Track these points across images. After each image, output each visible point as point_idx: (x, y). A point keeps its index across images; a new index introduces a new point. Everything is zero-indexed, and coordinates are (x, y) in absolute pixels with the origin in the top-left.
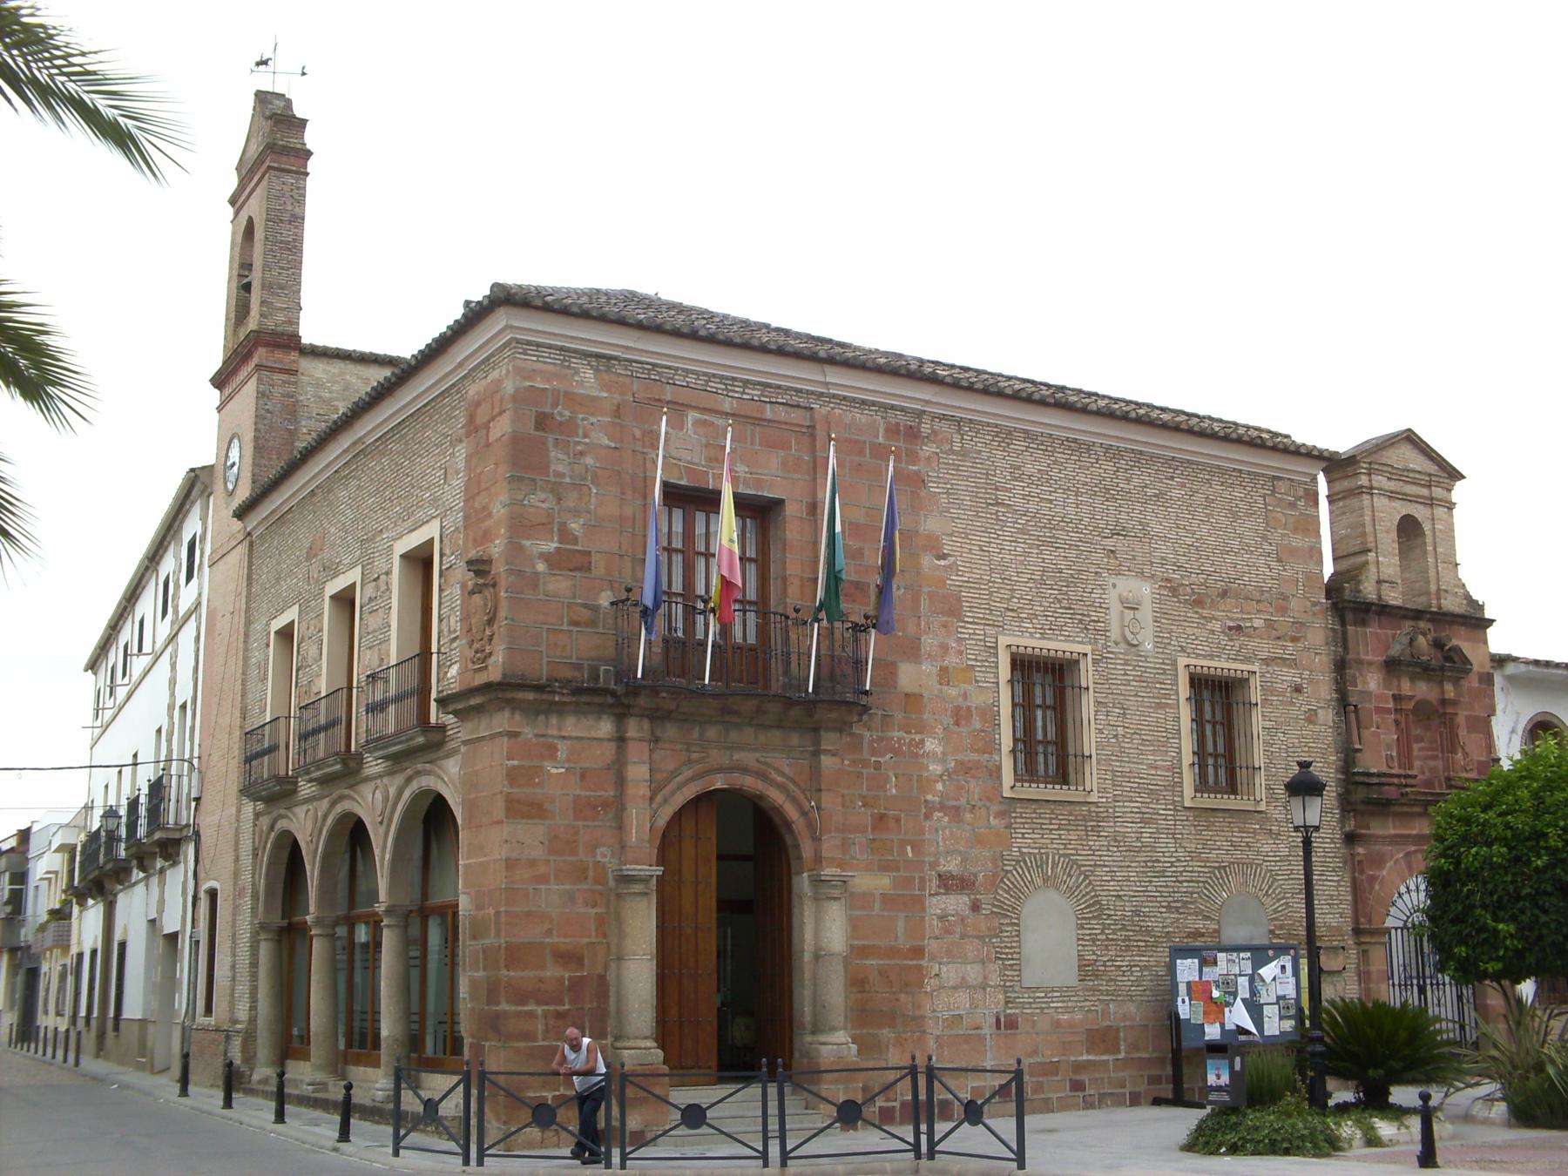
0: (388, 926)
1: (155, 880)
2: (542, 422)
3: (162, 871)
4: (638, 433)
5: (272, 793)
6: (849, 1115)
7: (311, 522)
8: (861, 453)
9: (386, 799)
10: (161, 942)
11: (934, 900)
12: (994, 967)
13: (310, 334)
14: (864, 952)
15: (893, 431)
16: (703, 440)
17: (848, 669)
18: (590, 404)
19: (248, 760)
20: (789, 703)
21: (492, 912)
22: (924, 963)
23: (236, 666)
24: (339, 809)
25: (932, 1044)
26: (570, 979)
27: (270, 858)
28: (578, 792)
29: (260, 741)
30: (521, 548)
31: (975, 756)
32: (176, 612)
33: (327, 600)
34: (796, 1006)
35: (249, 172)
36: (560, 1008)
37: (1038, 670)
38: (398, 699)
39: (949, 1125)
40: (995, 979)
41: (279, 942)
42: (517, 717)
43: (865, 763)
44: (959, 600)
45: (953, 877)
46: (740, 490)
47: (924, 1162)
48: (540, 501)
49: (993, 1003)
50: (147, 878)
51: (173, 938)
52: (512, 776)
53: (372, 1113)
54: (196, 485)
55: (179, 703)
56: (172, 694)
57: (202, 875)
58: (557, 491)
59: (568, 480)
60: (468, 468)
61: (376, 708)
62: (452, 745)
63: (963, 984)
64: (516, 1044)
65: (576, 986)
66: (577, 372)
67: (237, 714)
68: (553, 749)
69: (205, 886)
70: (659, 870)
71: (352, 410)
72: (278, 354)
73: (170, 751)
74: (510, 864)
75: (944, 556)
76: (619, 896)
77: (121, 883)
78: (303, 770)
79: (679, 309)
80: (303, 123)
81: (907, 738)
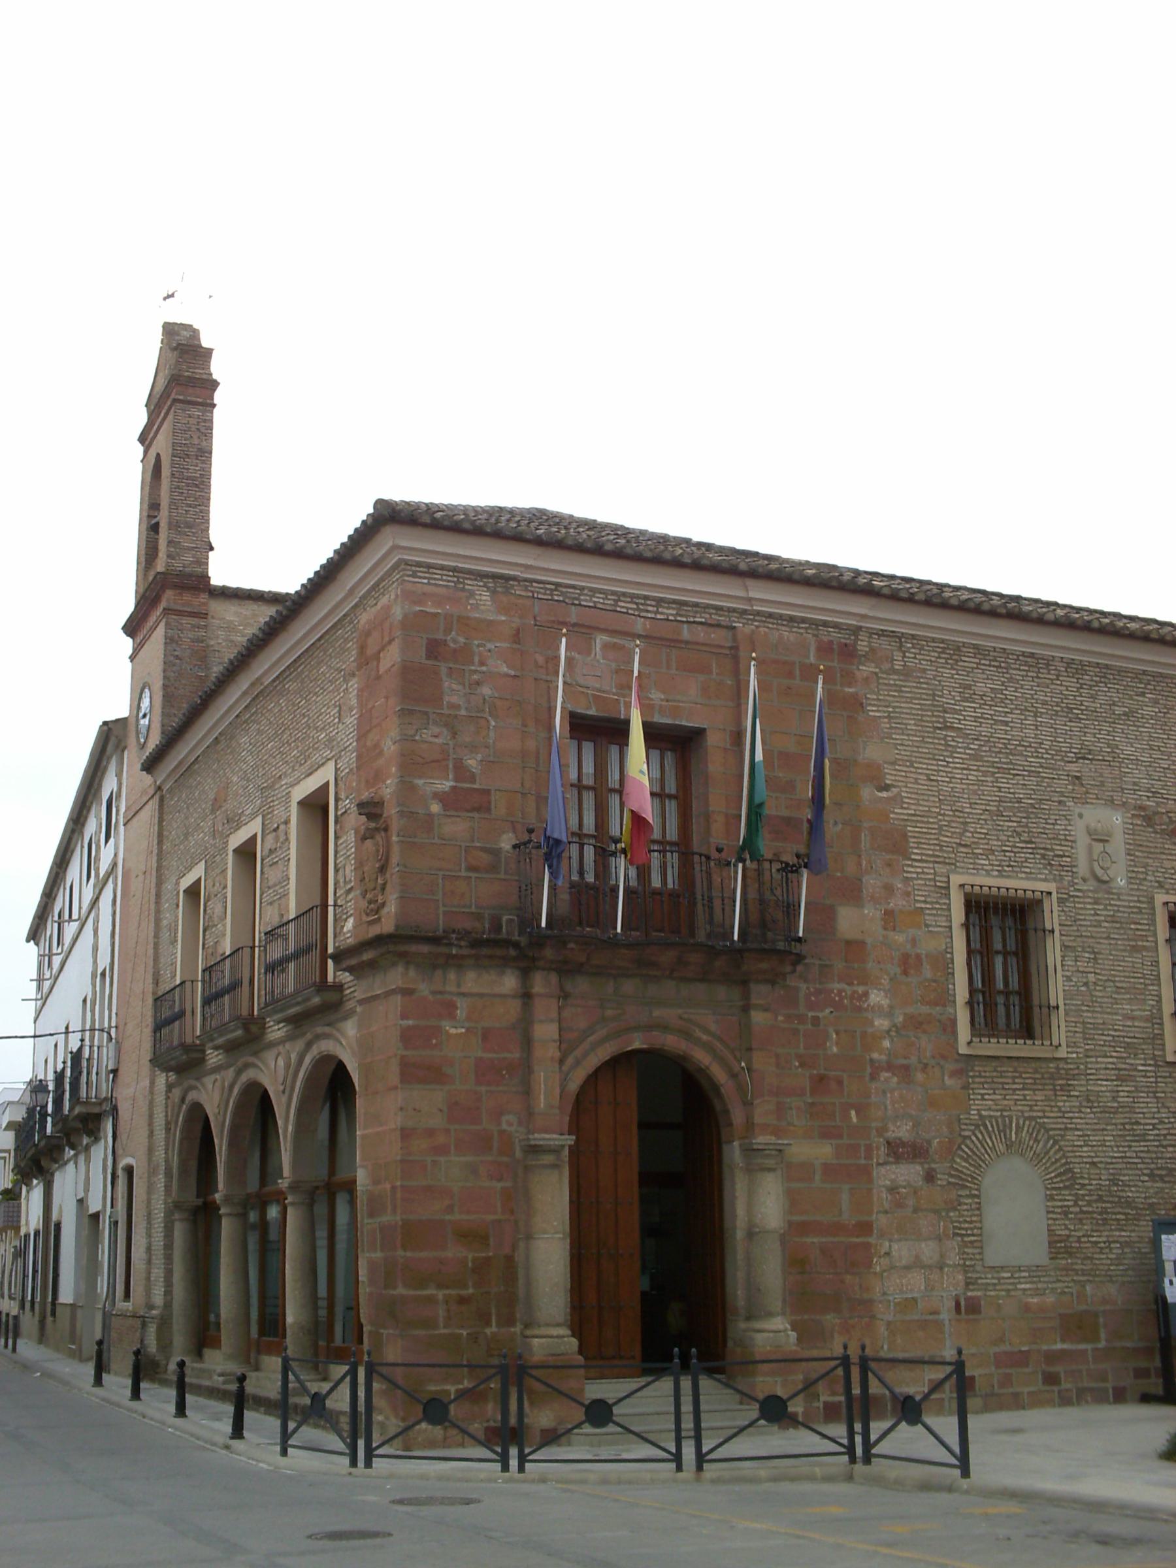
0: (292, 1204)
1: (82, 1158)
2: (434, 649)
3: (87, 1148)
4: (541, 659)
5: (180, 1061)
6: (775, 1411)
7: (216, 772)
8: (790, 675)
9: (288, 1066)
10: (86, 1220)
11: (883, 1170)
12: (953, 1244)
13: (221, 573)
14: (803, 1228)
15: (825, 649)
16: (614, 665)
17: (779, 915)
18: (486, 628)
19: (157, 1028)
20: (712, 952)
21: (388, 1186)
22: (872, 1240)
23: (149, 929)
24: (244, 1078)
25: (882, 1330)
26: (474, 1260)
27: (181, 1132)
28: (480, 1054)
29: (172, 1007)
30: (413, 788)
31: (925, 1009)
32: (97, 875)
33: (230, 853)
34: (728, 1289)
35: (158, 405)
36: (463, 1292)
37: (996, 912)
38: (296, 956)
39: (886, 1425)
40: (953, 1258)
41: (195, 1222)
42: (412, 973)
43: (801, 1019)
44: (905, 836)
45: (903, 1144)
46: (657, 719)
47: (859, 1467)
48: (433, 736)
49: (951, 1285)
50: (76, 1155)
51: (95, 1217)
52: (407, 1037)
53: (263, 1404)
54: (111, 738)
55: (100, 971)
56: (95, 962)
57: (119, 1152)
58: (451, 724)
59: (463, 712)
60: (361, 704)
61: (272, 968)
62: (350, 1005)
63: (916, 1264)
64: (416, 1332)
65: (481, 1268)
66: (472, 594)
67: (150, 980)
68: (451, 1006)
69: (123, 1162)
70: (570, 1140)
71: (248, 649)
72: (187, 597)
73: (93, 1021)
74: (406, 1134)
75: (886, 788)
76: (527, 1169)
77: (56, 1161)
78: (208, 1036)
79: (591, 525)
80: (209, 352)
81: (849, 990)
